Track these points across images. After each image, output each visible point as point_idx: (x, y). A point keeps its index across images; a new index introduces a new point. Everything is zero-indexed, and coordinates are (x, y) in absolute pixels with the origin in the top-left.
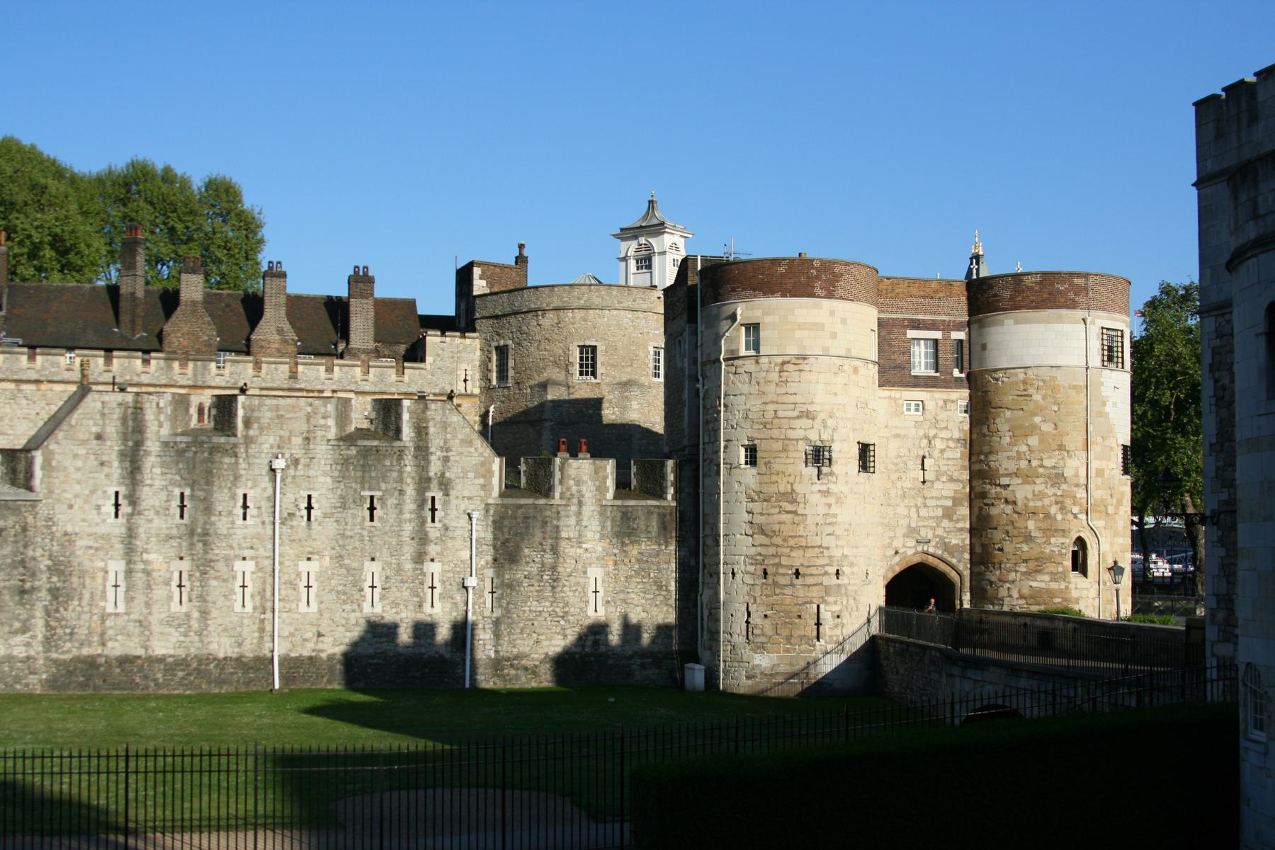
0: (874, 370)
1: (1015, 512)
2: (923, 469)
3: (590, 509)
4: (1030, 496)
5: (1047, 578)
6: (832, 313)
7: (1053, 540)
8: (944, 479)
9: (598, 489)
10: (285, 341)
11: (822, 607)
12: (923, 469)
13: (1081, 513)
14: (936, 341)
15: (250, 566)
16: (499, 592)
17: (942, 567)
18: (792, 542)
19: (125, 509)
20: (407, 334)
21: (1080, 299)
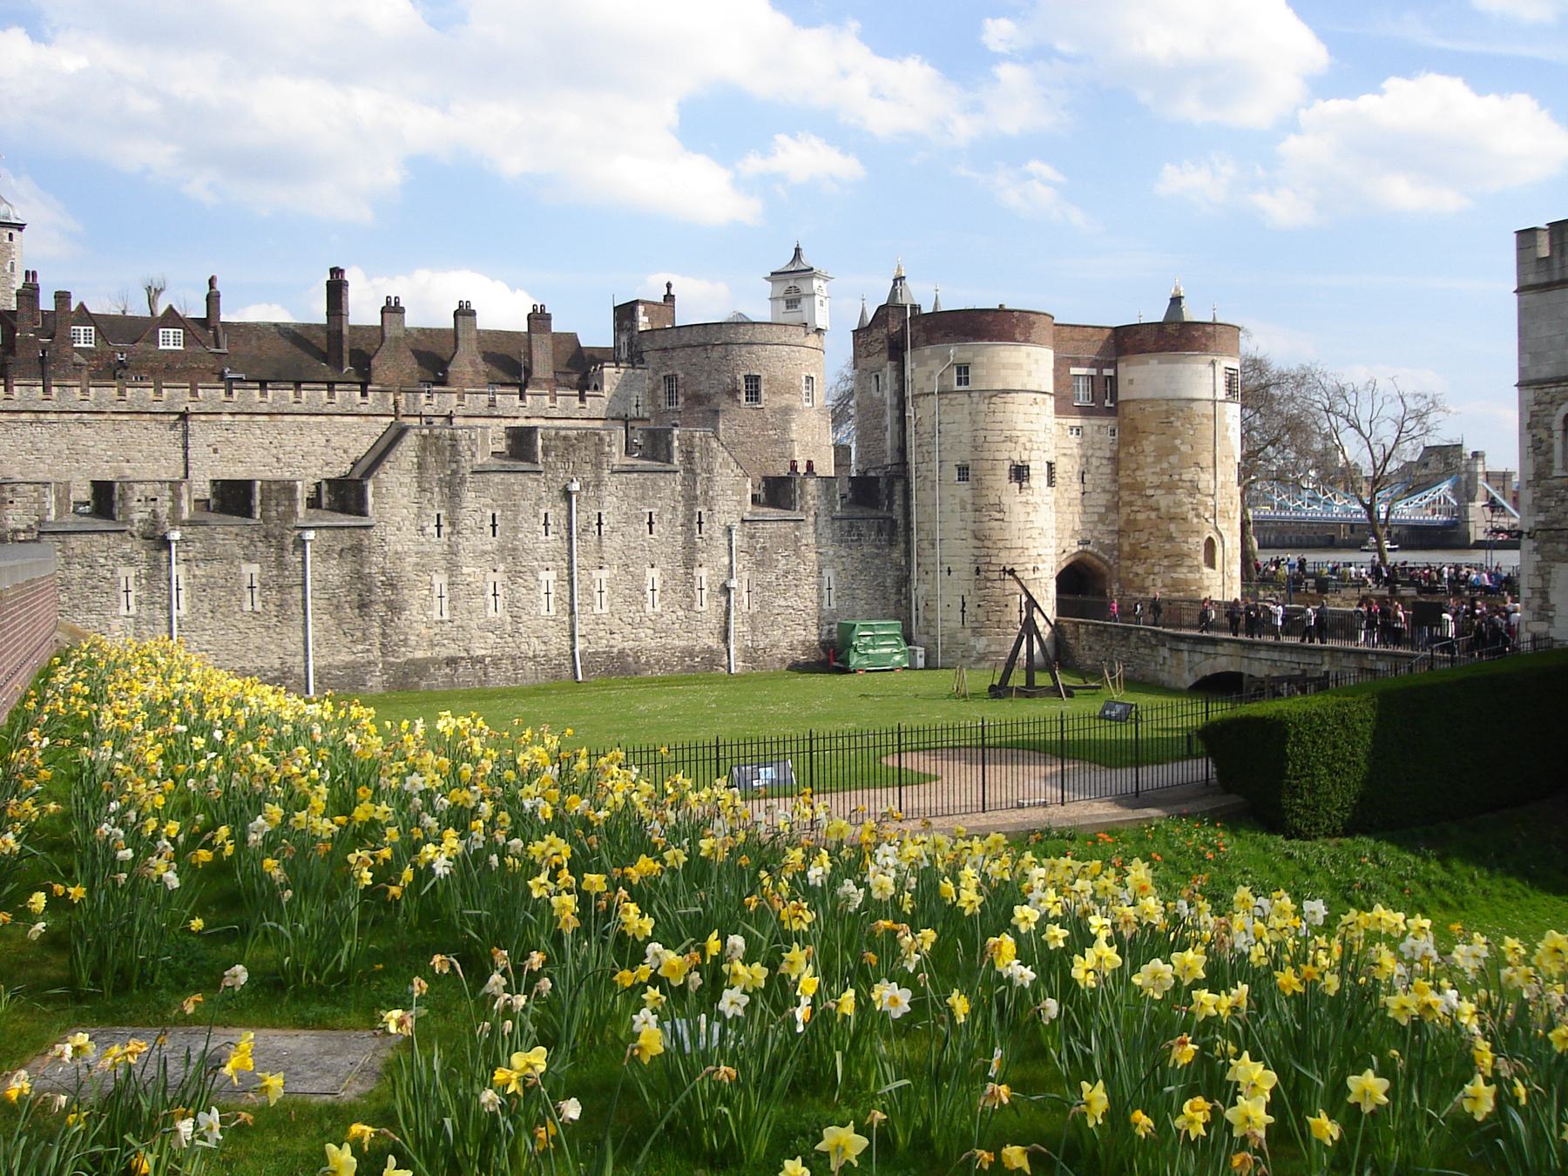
0: (1051, 402)
10: (477, 372)
15: (552, 575)
18: (1000, 544)
19: (446, 529)
20: (580, 367)
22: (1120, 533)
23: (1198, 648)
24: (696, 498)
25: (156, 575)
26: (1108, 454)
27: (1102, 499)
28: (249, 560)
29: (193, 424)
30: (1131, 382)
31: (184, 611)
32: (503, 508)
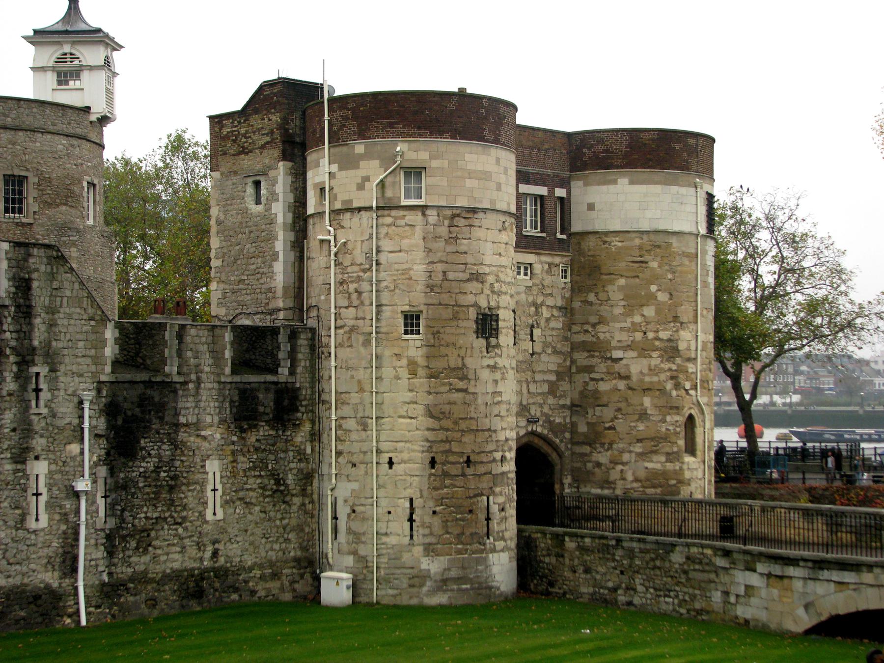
1: (630, 388)
2: (532, 340)
3: (209, 386)
4: (646, 371)
5: (663, 459)
6: (498, 160)
7: (668, 418)
8: (549, 351)
11: (491, 498)
12: (532, 340)
13: (691, 389)
14: (542, 197)
16: (114, 496)
17: (546, 448)
18: (463, 425)
21: (693, 161)
22: (574, 408)
23: (825, 574)
27: (550, 362)
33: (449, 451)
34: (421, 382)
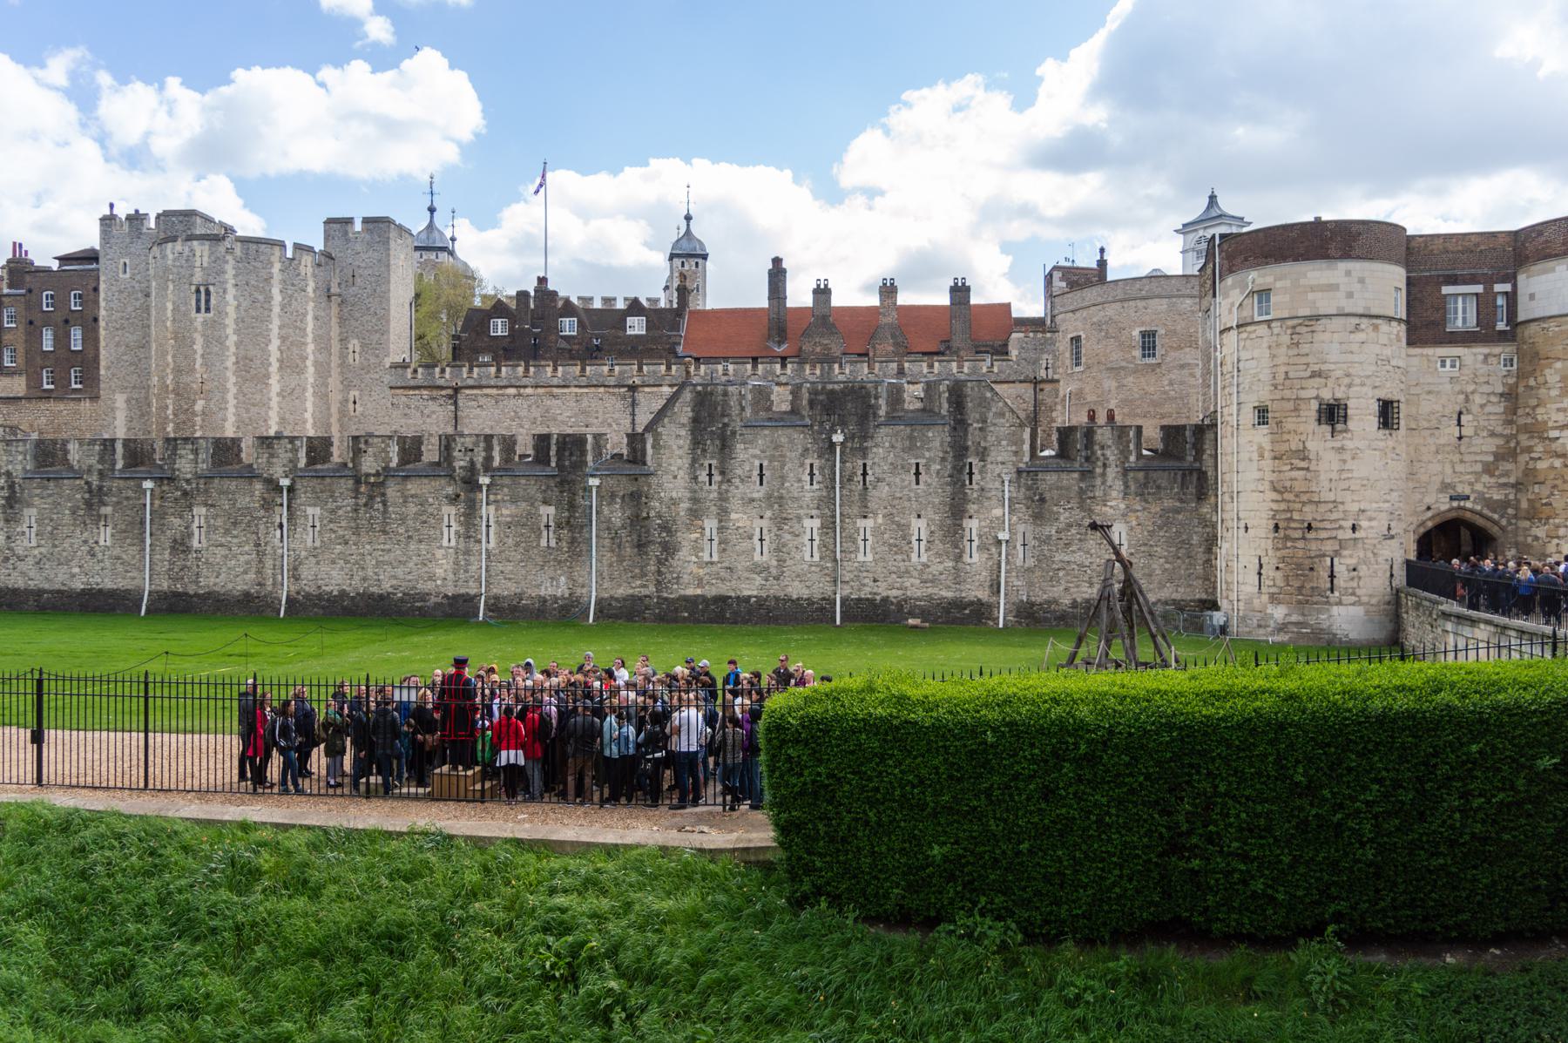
2: (1459, 424)
6: (1348, 273)
9: (1122, 452)
11: (1336, 560)
12: (1459, 424)
15: (816, 523)
18: (1304, 498)
19: (717, 478)
22: (1518, 486)
24: (967, 449)
25: (470, 515)
26: (1500, 389)
28: (546, 502)
29: (639, 396)
30: (1532, 297)
31: (492, 545)
32: (772, 459)
33: (1291, 519)
34: (1268, 464)
